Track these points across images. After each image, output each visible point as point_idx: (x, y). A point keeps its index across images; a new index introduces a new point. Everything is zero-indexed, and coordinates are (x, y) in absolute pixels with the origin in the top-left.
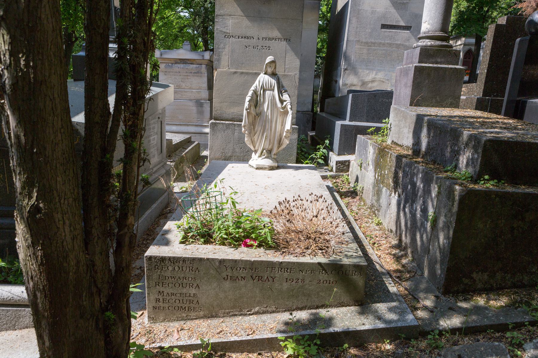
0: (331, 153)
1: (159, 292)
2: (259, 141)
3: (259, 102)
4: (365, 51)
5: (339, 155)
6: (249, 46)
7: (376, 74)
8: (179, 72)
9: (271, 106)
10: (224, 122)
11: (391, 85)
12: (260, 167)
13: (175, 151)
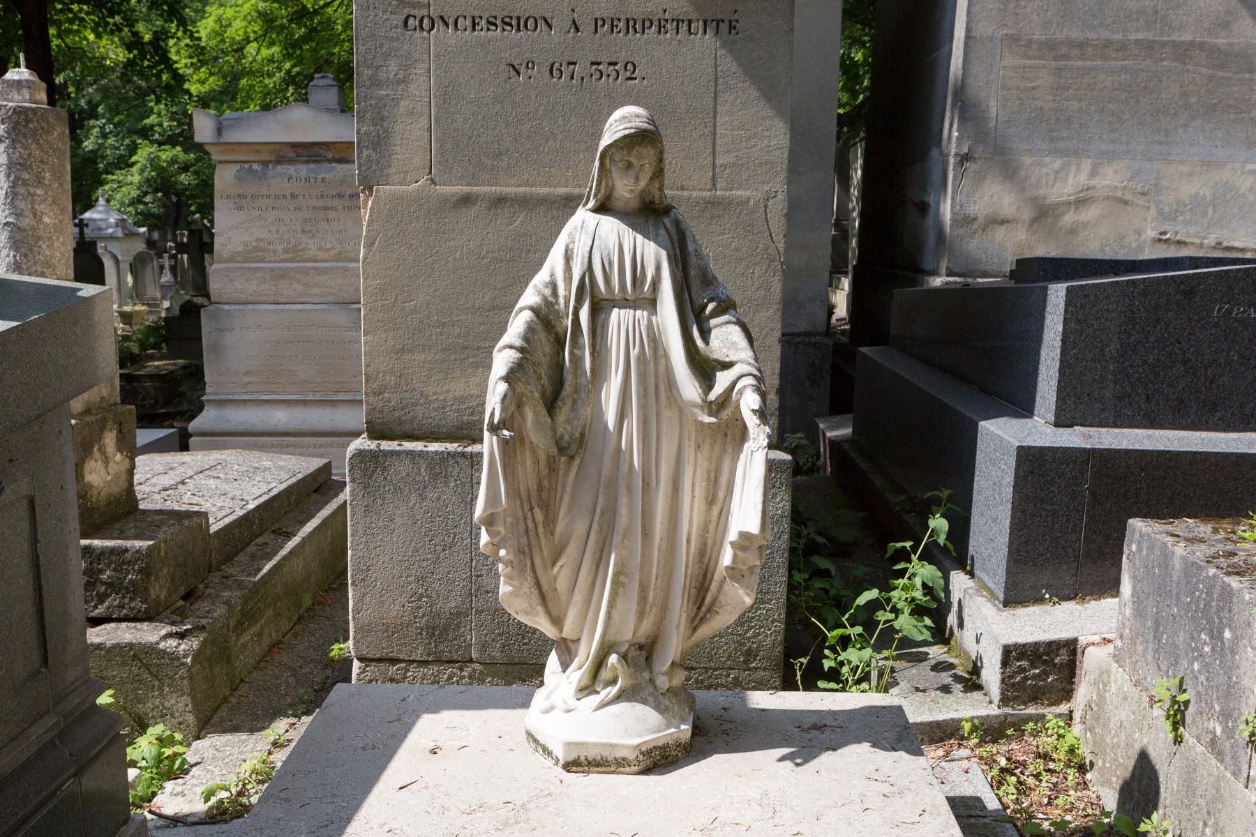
0: (959, 579)
2: (578, 597)
3: (569, 378)
4: (1044, 79)
5: (1014, 597)
6: (530, 64)
7: (1093, 173)
8: (293, 196)
9: (643, 395)
10: (417, 446)
11: (1160, 213)
12: (592, 754)
13: (229, 558)
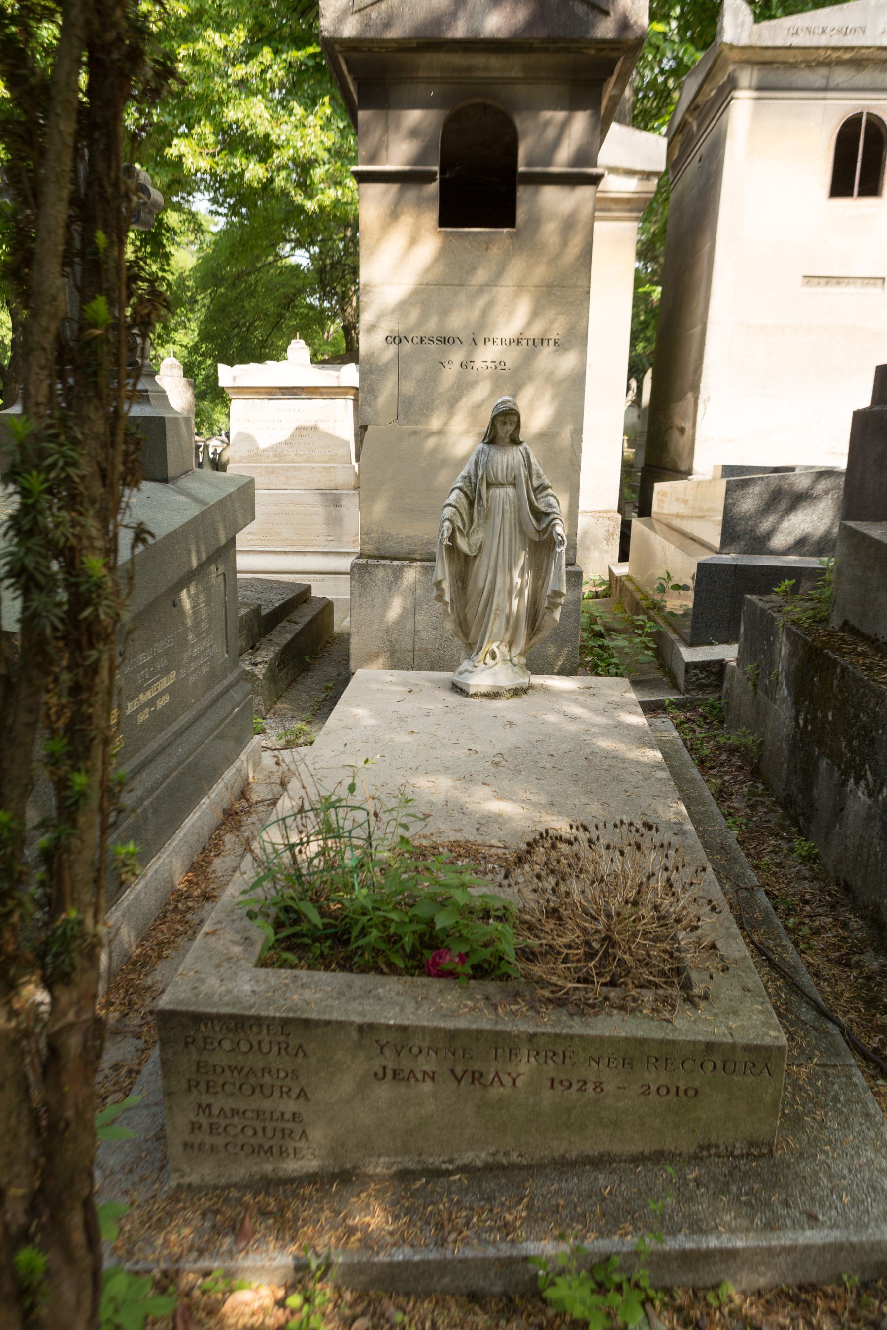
1: (200, 1106)
